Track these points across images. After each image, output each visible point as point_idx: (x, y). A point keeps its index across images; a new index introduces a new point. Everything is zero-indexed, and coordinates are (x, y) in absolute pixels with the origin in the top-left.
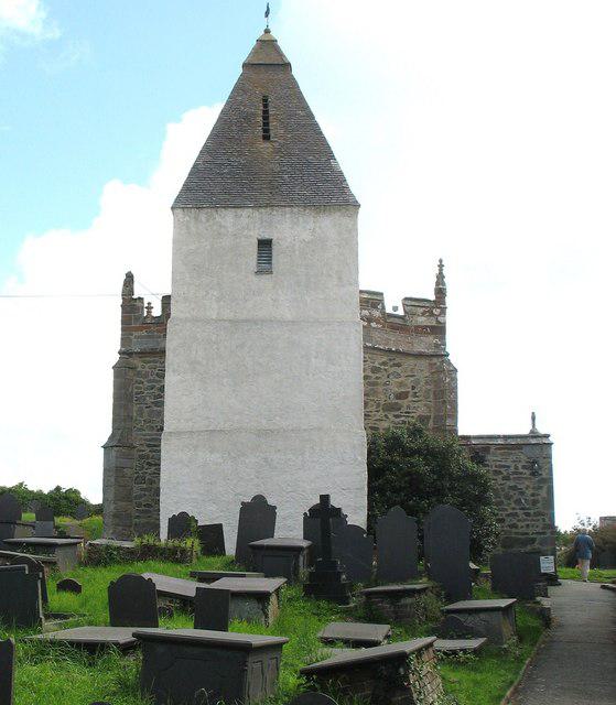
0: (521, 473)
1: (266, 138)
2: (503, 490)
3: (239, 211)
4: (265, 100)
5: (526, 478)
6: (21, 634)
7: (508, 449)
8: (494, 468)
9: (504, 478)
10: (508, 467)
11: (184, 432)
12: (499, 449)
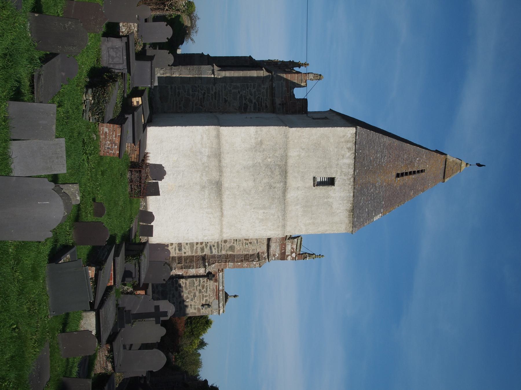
0: (203, 299)
2: (194, 290)
3: (352, 166)
4: (422, 171)
7: (216, 292)
9: (200, 290)
10: (206, 292)
11: (220, 161)
12: (216, 288)
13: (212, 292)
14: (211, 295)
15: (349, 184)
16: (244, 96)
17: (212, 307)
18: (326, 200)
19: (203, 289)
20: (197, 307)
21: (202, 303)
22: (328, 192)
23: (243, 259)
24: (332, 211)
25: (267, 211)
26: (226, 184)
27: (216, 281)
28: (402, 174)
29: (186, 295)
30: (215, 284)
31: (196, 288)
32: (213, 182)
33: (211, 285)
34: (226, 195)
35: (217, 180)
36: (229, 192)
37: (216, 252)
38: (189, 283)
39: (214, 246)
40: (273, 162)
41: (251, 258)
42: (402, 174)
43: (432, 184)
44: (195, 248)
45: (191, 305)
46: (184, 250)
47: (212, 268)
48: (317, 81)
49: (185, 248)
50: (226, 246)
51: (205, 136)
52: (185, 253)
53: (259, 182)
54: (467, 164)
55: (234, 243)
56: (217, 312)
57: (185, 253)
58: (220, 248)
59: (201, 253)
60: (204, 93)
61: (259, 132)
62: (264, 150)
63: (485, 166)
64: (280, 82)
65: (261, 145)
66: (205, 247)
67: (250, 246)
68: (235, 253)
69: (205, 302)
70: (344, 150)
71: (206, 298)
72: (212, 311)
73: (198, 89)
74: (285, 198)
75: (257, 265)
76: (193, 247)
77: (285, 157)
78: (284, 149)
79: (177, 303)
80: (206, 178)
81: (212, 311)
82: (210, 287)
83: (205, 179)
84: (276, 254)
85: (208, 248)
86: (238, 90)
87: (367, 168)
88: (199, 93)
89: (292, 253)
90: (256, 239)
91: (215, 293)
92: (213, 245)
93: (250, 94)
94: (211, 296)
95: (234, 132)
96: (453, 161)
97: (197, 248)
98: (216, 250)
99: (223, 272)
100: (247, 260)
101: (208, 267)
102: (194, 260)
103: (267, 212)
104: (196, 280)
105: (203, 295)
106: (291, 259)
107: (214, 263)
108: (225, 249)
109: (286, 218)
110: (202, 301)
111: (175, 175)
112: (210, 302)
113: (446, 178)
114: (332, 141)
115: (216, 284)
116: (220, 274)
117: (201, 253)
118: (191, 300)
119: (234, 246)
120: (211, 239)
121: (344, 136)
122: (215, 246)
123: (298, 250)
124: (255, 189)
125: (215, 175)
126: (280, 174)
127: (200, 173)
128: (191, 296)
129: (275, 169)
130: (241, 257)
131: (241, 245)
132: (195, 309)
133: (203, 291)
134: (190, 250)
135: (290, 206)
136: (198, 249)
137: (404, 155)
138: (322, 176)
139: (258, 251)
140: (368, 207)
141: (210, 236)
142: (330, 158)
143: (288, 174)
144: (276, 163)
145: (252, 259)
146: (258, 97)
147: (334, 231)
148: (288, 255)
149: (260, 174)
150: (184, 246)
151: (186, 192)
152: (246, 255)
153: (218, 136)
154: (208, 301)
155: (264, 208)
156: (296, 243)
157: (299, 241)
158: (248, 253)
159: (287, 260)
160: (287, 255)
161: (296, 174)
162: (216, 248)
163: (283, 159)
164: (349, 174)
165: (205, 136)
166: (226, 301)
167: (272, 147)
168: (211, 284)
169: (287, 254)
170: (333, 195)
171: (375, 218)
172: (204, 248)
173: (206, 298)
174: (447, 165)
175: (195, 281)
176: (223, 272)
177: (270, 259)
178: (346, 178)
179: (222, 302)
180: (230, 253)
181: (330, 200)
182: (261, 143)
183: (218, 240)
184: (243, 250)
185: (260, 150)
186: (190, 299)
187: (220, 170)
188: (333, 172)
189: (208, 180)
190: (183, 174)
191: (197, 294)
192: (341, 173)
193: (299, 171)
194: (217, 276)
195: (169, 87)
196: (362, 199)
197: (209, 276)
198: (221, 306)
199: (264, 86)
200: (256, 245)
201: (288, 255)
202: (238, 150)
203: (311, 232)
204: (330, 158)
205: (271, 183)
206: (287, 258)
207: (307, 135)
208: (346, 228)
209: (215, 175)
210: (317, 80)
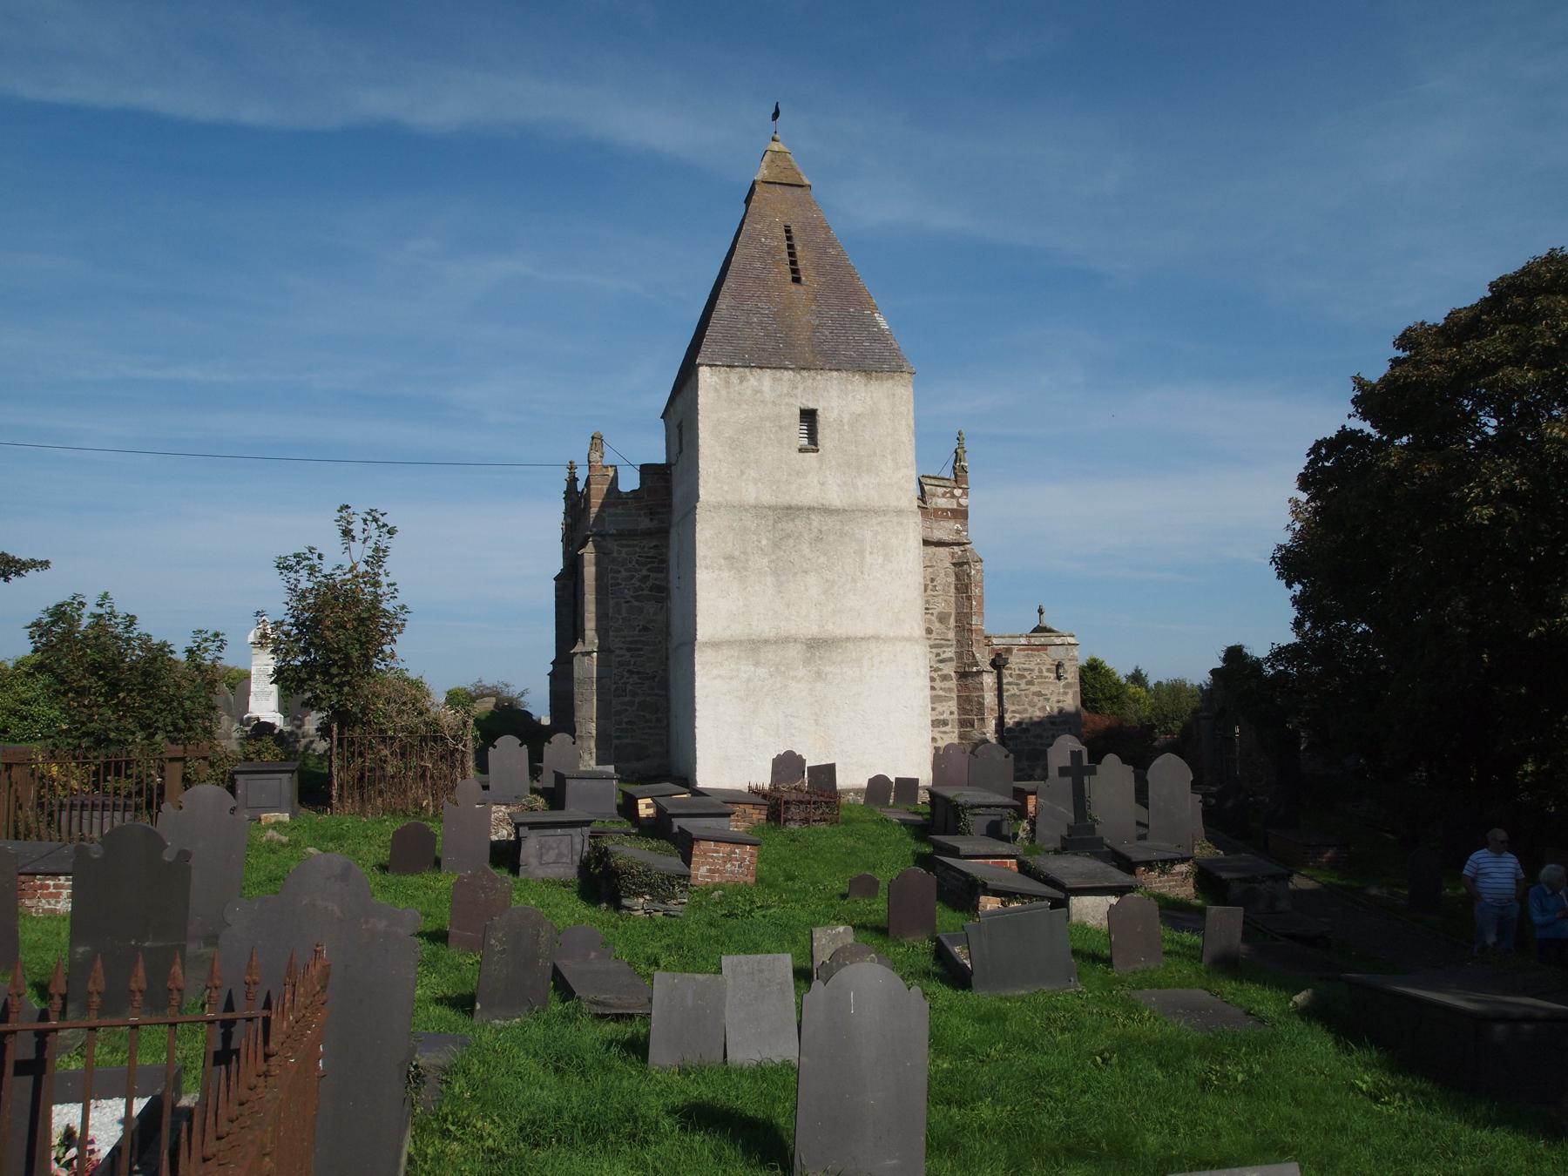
1: (796, 280)
3: (778, 373)
4: (788, 231)
5: (1051, 683)
6: (144, 802)
8: (1018, 672)
10: (1032, 670)
11: (766, 642)
12: (1024, 650)
18: (846, 427)
19: (1025, 677)
23: (964, 595)
26: (813, 630)
27: (1009, 650)
28: (794, 271)
32: (809, 655)
33: (1018, 661)
37: (949, 649)
38: (1013, 704)
39: (938, 655)
42: (794, 271)
44: (941, 693)
45: (1059, 702)
47: (984, 658)
52: (952, 713)
54: (774, 140)
55: (932, 614)
57: (952, 713)
58: (943, 642)
62: (744, 553)
65: (733, 558)
66: (940, 673)
72: (1070, 660)
76: (940, 696)
77: (759, 510)
81: (1070, 660)
85: (941, 666)
86: (623, 605)
88: (628, 683)
89: (953, 496)
97: (941, 689)
110: (1050, 680)
111: (793, 731)
114: (725, 415)
121: (716, 390)
123: (948, 484)
125: (794, 652)
126: (793, 520)
131: (936, 599)
132: (1065, 693)
133: (1029, 678)
136: (943, 687)
137: (755, 268)
139: (948, 565)
143: (794, 503)
145: (966, 577)
146: (637, 563)
152: (956, 588)
153: (716, 645)
155: (861, 553)
156: (933, 487)
157: (929, 481)
158: (953, 586)
159: (967, 506)
162: (942, 650)
166: (1050, 631)
168: (1016, 661)
169: (955, 507)
173: (1044, 670)
178: (801, 387)
180: (952, 621)
181: (846, 418)
182: (729, 558)
186: (1045, 703)
187: (784, 641)
190: (791, 716)
191: (1035, 689)
194: (1000, 649)
195: (617, 742)
197: (998, 664)
209: (794, 652)
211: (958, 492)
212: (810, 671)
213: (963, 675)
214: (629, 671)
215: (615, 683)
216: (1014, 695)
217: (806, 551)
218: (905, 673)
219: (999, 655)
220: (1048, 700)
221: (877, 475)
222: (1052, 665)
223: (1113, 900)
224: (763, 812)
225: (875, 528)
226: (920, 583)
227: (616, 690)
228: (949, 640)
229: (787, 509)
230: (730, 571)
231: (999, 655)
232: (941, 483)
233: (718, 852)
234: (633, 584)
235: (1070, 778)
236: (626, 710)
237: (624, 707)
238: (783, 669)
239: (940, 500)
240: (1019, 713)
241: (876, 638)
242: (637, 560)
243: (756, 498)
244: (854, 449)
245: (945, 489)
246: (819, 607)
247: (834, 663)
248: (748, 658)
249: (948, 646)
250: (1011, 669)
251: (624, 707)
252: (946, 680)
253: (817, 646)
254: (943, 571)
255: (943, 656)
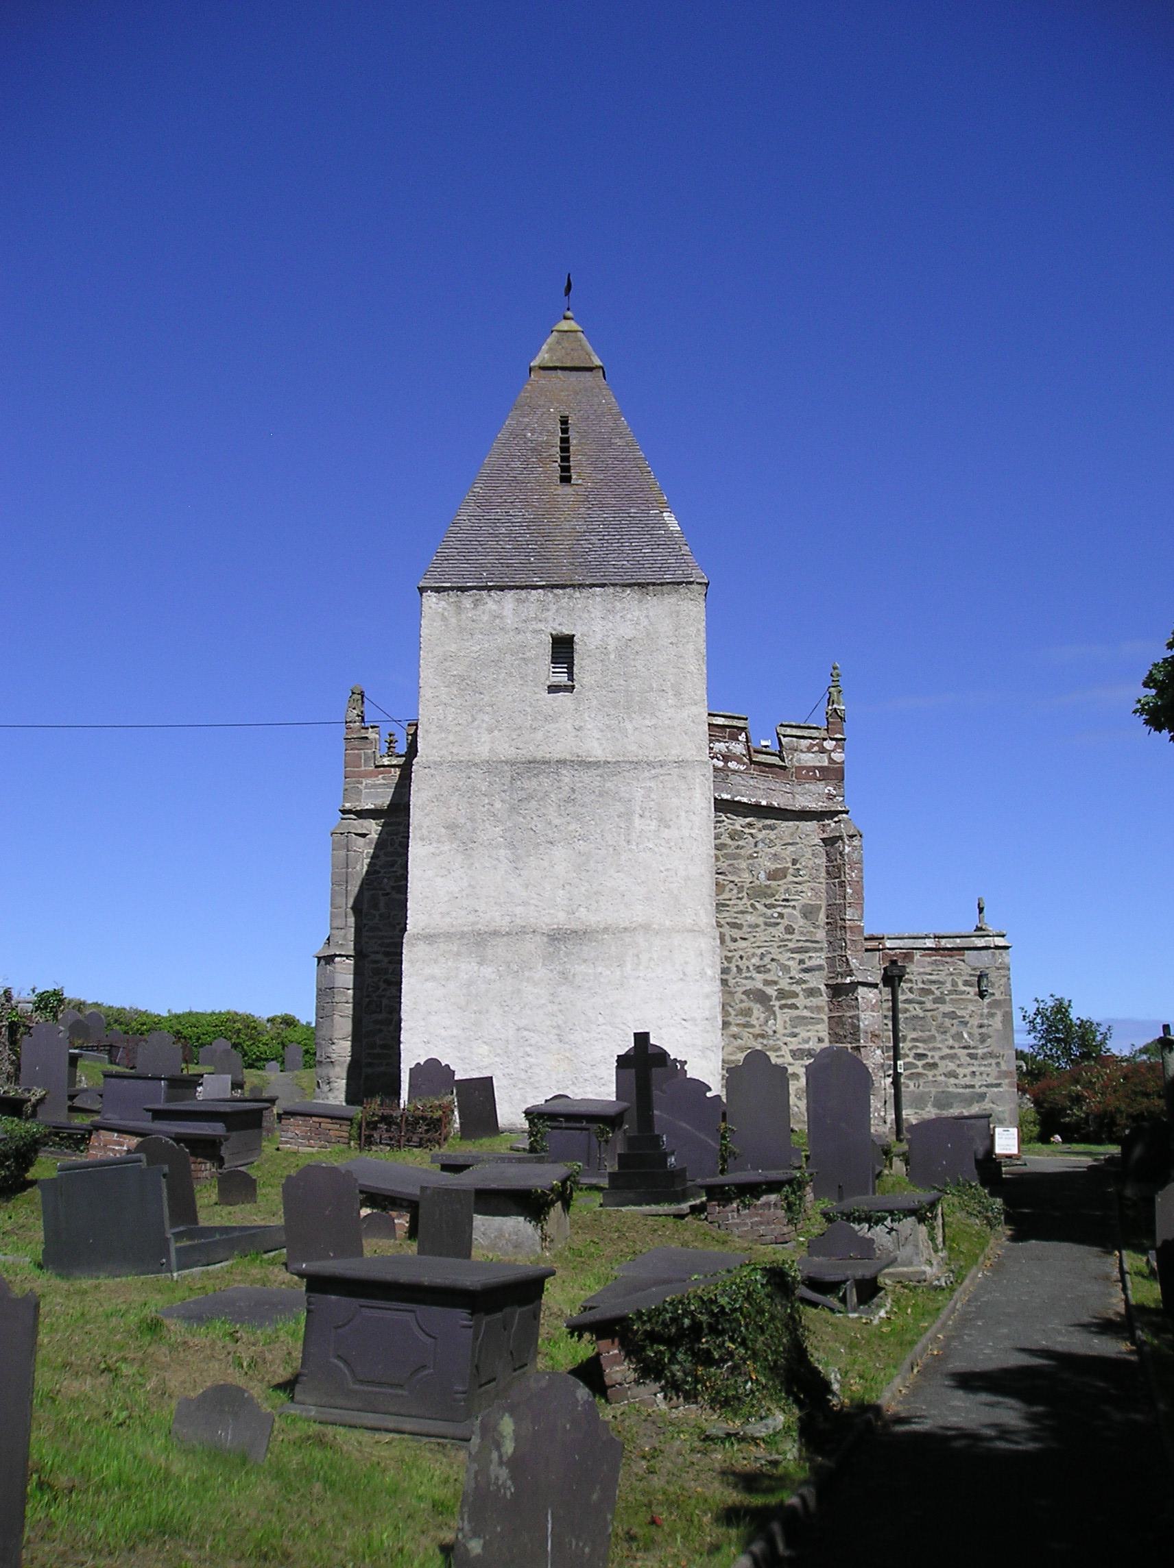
0: (963, 992)
4: (564, 421)
5: (971, 1001)
9: (935, 1001)
11: (495, 933)
12: (930, 956)
13: (941, 968)
14: (951, 969)
15: (571, 597)
16: (396, 882)
17: (987, 968)
18: (612, 657)
19: (933, 993)
20: (986, 1011)
21: (975, 995)
22: (591, 651)
23: (837, 880)
24: (642, 639)
25: (638, 808)
26: (561, 918)
27: (908, 955)
28: (566, 469)
29: (951, 1041)
30: (918, 959)
31: (930, 1010)
32: (551, 950)
33: (922, 970)
34: (588, 917)
35: (545, 939)
36: (582, 909)
37: (818, 954)
38: (914, 1030)
39: (801, 962)
40: (503, 794)
41: (836, 859)
42: (566, 469)
43: (603, 396)
44: (806, 1013)
45: (981, 1026)
46: (811, 1043)
47: (869, 968)
48: (365, 700)
49: (807, 1041)
50: (801, 929)
51: (428, 971)
52: (820, 1040)
53: (555, 830)
55: (794, 907)
56: (1001, 954)
57: (820, 1040)
58: (808, 944)
59: (821, 995)
60: (386, 981)
61: (424, 831)
62: (472, 820)
63: (569, 275)
64: (364, 791)
65: (457, 826)
66: (804, 986)
67: (803, 864)
68: (824, 904)
69: (970, 986)
70: (480, 615)
71: (960, 983)
72: (998, 969)
73: (375, 999)
74: (602, 763)
75: (854, 843)
76: (805, 1018)
77: (491, 767)
78: (471, 768)
79: (973, 1065)
80: (539, 968)
81: (998, 969)
82: (927, 974)
83: (540, 972)
84: (827, 791)
85: (806, 976)
86: (382, 898)
87: (532, 556)
88: (384, 996)
89: (823, 751)
90: (784, 847)
91: (944, 959)
92: (799, 964)
93: (392, 866)
94: (954, 969)
95: (420, 896)
96: (550, 350)
97: (806, 1007)
98: (814, 955)
99: (883, 938)
100: (839, 868)
101: (856, 976)
102: (839, 1017)
103: (641, 808)
104: (906, 1013)
105: (950, 992)
106: (840, 753)
107: (847, 959)
108: (812, 932)
109: (660, 758)
110: (969, 996)
111: (528, 1049)
112: (973, 972)
113: (593, 362)
114: (453, 648)
115: (919, 957)
116: (888, 945)
117: (821, 995)
118: (966, 1027)
119: (803, 906)
120: (711, 958)
121: (444, 619)
122: (803, 957)
123: (815, 733)
124: (574, 842)
125: (532, 945)
126: (536, 776)
127: (525, 984)
128: (953, 1025)
129: (522, 789)
130: (832, 886)
131: (800, 888)
132: (992, 1015)
133: (937, 993)
134: (811, 1027)
135: (625, 748)
136: (809, 1004)
137: (513, 469)
138: (547, 671)
139: (817, 841)
140: (640, 548)
141: (702, 961)
142: (500, 650)
143: (539, 755)
144: (506, 787)
145: (839, 857)
146: (400, 845)
147: (699, 630)
148: (830, 758)
149: (534, 828)
150: (800, 1043)
151: (576, 1023)
152: (828, 873)
153: (429, 938)
154: (968, 979)
155: (627, 816)
156: (794, 739)
157: (789, 731)
158: (823, 870)
159: (843, 762)
160: (829, 763)
161: (539, 735)
162: (808, 955)
163: (497, 768)
164: (544, 601)
165: (428, 971)
167: (465, 799)
168: (917, 969)
169: (826, 764)
170: (599, 636)
171: (671, 528)
172: (808, 988)
173: (960, 983)
174: (557, 365)
175: (907, 1015)
176: (883, 938)
177: (840, 809)
178: (554, 607)
179: (973, 939)
180: (822, 918)
181: (612, 643)
182: (452, 827)
183: (714, 939)
184: (815, 882)
185: (469, 828)
186: (961, 1028)
187: (519, 933)
188: (536, 641)
189: (544, 965)
190: (526, 1030)
191: (947, 1008)
192: (540, 621)
193: (531, 727)
194: (895, 955)
195: (369, 1070)
196: (614, 563)
197: (893, 978)
198: (985, 941)
199: (373, 833)
200: (801, 848)
201: (830, 758)
202: (470, 885)
203: (701, 692)
204: (500, 650)
205: (559, 800)
206: (838, 763)
207: (438, 710)
208: (692, 600)
209: (532, 945)
210: (363, 702)
211: (829, 745)
212: (551, 971)
213: (837, 991)
214: (386, 981)
215: (368, 996)
216: (916, 1017)
217: (552, 813)
218: (684, 974)
219: (894, 962)
220: (966, 1023)
221: (653, 714)
222: (971, 975)
223: (140, 1139)
224: (344, 1128)
225: (648, 784)
226: (709, 855)
227: (369, 1003)
228: (817, 942)
229: (530, 762)
230: (452, 843)
231: (894, 962)
232: (805, 733)
233: (121, 1145)
234: (396, 872)
235: (634, 1070)
236: (380, 1031)
237: (378, 1027)
238: (516, 968)
239: (804, 755)
240: (924, 1041)
241: (646, 928)
242: (400, 842)
243: (491, 750)
244: (622, 682)
245: (810, 741)
246: (567, 887)
247: (585, 961)
248: (471, 953)
249: (816, 950)
250: (911, 981)
251: (378, 1027)
252: (813, 996)
253: (558, 938)
254: (809, 850)
255: (808, 964)
